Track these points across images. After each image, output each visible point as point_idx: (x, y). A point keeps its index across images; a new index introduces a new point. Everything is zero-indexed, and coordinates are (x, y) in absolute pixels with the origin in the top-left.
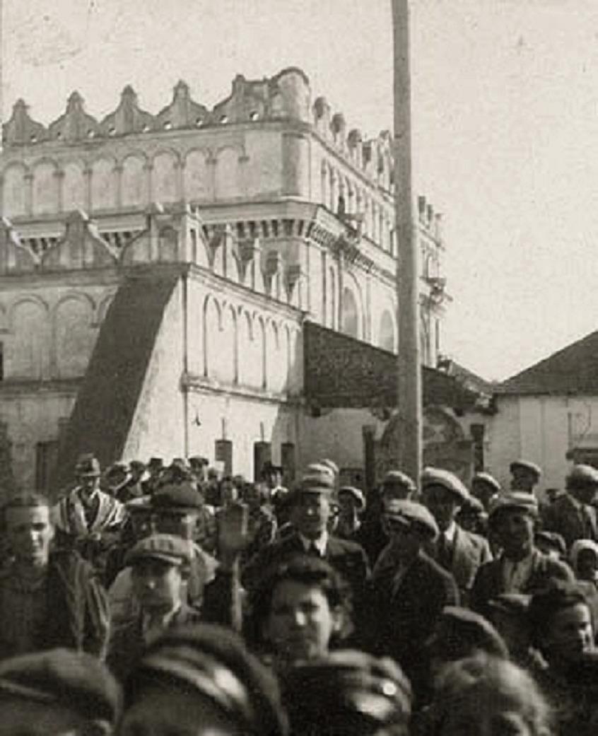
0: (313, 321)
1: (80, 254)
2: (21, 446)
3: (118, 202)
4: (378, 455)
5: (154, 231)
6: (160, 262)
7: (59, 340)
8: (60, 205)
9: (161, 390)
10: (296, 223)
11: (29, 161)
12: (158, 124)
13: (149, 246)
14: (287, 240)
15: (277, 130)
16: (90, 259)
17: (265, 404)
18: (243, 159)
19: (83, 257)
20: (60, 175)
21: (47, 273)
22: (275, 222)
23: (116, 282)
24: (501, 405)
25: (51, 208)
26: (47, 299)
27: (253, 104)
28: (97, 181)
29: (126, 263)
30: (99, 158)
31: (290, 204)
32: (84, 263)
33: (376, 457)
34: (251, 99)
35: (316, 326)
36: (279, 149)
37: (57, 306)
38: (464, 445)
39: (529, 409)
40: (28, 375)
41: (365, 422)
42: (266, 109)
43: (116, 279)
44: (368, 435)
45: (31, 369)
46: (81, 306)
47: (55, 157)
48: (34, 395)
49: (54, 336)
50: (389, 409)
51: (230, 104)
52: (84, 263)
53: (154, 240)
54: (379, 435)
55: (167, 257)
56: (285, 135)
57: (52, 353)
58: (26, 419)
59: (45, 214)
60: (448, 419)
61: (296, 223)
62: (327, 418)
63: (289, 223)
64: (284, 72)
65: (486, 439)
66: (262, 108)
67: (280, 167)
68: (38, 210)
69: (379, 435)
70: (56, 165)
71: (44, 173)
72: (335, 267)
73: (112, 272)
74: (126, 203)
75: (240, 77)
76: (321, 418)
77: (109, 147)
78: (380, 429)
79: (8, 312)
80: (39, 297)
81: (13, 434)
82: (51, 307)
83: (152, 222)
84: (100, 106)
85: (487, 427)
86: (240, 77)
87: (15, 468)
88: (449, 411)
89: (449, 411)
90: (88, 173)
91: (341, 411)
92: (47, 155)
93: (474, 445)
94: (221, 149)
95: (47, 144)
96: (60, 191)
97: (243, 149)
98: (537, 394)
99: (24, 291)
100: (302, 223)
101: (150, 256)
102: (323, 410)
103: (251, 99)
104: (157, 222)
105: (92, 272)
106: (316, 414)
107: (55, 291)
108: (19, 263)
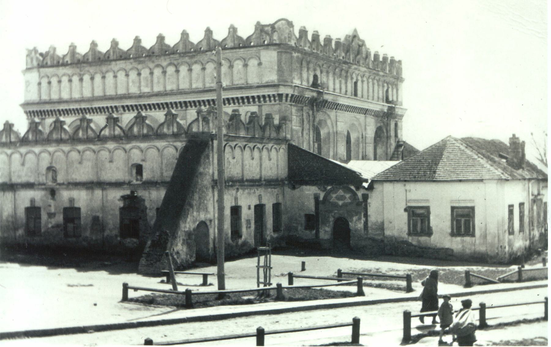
0: (294, 144)
1: (171, 128)
2: (150, 209)
3: (204, 85)
4: (321, 207)
5: (200, 119)
6: (203, 133)
7: (164, 164)
8: (178, 86)
9: (200, 190)
10: (284, 96)
11: (164, 64)
12: (223, 45)
13: (199, 126)
14: (280, 104)
15: (275, 50)
16: (175, 130)
17: (402, 126)
18: (260, 64)
19: (173, 129)
20: (177, 71)
21: (160, 136)
22: (274, 96)
23: (185, 141)
24: (376, 186)
25: (174, 87)
26: (160, 147)
27: (264, 37)
28: (194, 74)
29: (189, 132)
30: (196, 62)
31: (281, 86)
32: (173, 132)
33: (320, 208)
34: (263, 34)
35: (294, 146)
36: (276, 58)
37: (163, 150)
38: (359, 204)
39: (388, 188)
40: (153, 179)
41: (315, 192)
42: (270, 39)
43: (185, 139)
44: (316, 198)
45: (154, 177)
46: (172, 150)
47: (176, 62)
48: (154, 188)
49: (162, 163)
50: (326, 186)
51: (254, 37)
52: (173, 132)
53: (201, 123)
54: (321, 198)
55: (206, 130)
56: (278, 52)
57: (161, 169)
58: (152, 198)
59: (172, 90)
60: (351, 191)
61: (284, 96)
62: (298, 190)
63: (280, 96)
64: (279, 20)
65: (369, 201)
66: (268, 38)
67: (276, 67)
68: (169, 88)
69: (321, 198)
70: (176, 66)
71: (171, 70)
72: (311, 113)
73: (183, 135)
74: (208, 85)
75: (258, 23)
76: (296, 190)
77: (198, 58)
78: (322, 196)
79: (144, 152)
80: (155, 146)
81: (147, 204)
82: (161, 151)
83: (200, 115)
84: (196, 37)
85: (369, 195)
86: (258, 23)
87: (148, 218)
88: (353, 188)
89: (353, 188)
90: (190, 70)
91: (304, 187)
92: (172, 61)
93: (363, 204)
94: (249, 59)
95: (172, 56)
96: (178, 79)
97: (259, 59)
98: (391, 181)
99: (150, 144)
100: (287, 95)
101: (199, 129)
102: (297, 186)
103: (263, 34)
104: (202, 115)
105: (175, 136)
106: (294, 188)
107: (161, 144)
108: (148, 131)
